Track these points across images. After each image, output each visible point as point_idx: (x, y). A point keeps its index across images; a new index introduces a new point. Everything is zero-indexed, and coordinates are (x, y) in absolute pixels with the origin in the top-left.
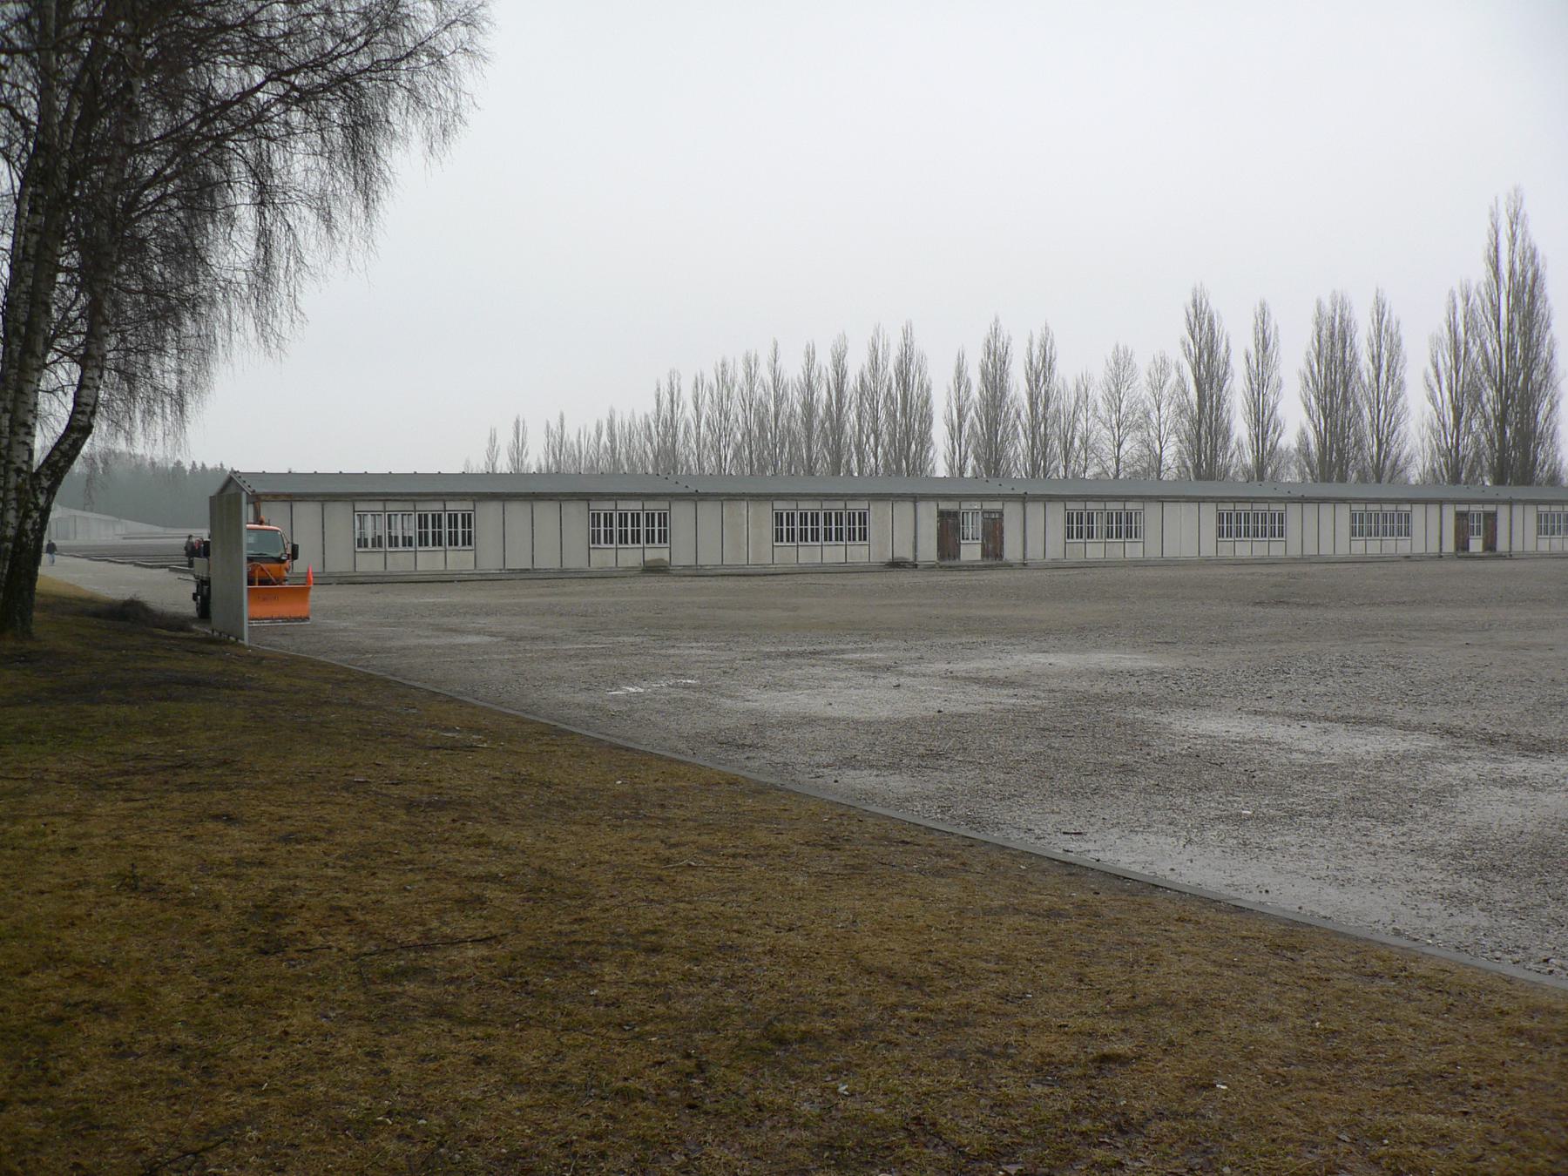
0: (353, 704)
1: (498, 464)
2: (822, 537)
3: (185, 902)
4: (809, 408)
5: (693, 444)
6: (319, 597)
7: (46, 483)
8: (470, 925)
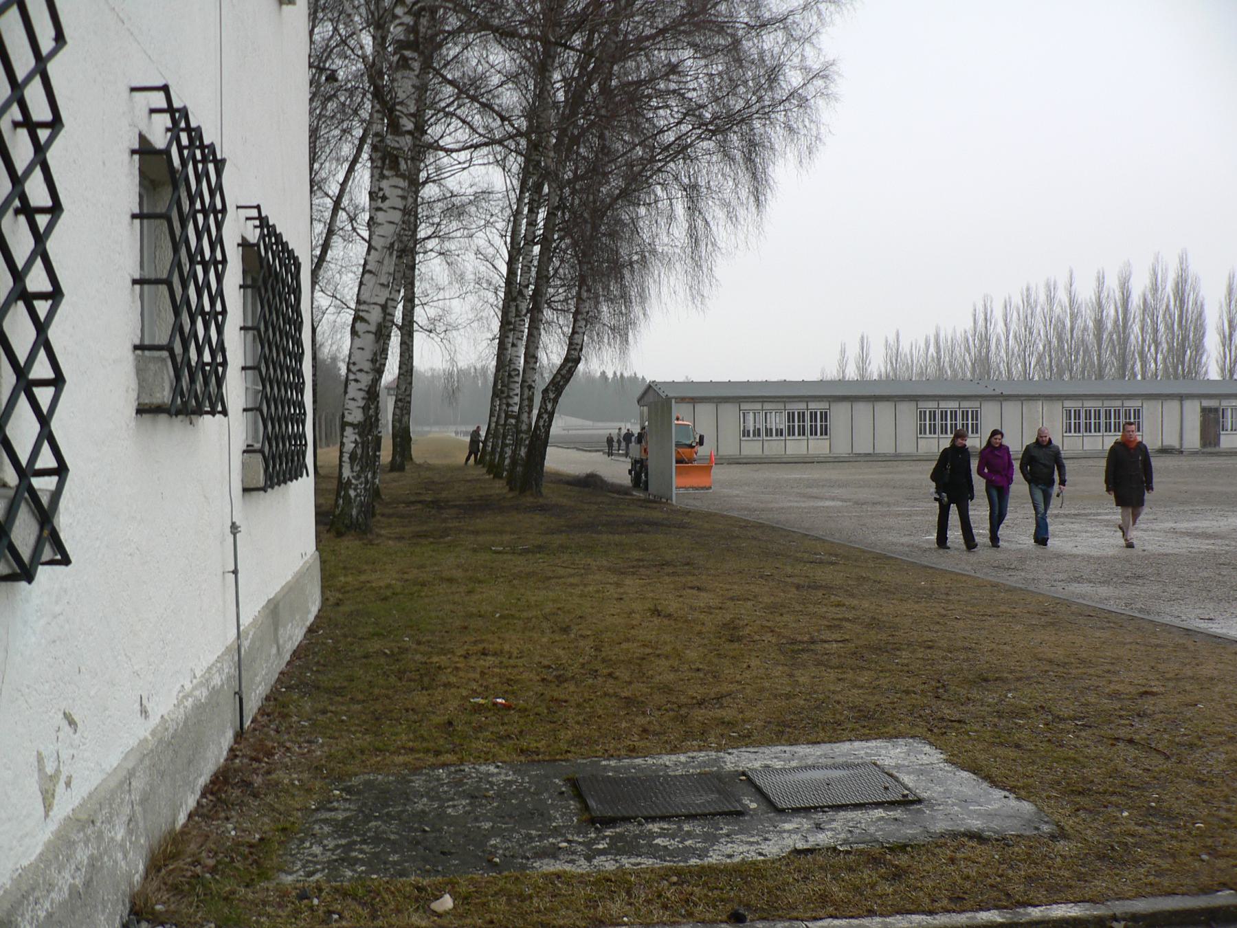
0: (754, 538)
1: (847, 371)
2: (1103, 428)
3: (686, 621)
4: (1099, 323)
5: (1003, 353)
6: (718, 473)
7: (552, 396)
8: (837, 636)
